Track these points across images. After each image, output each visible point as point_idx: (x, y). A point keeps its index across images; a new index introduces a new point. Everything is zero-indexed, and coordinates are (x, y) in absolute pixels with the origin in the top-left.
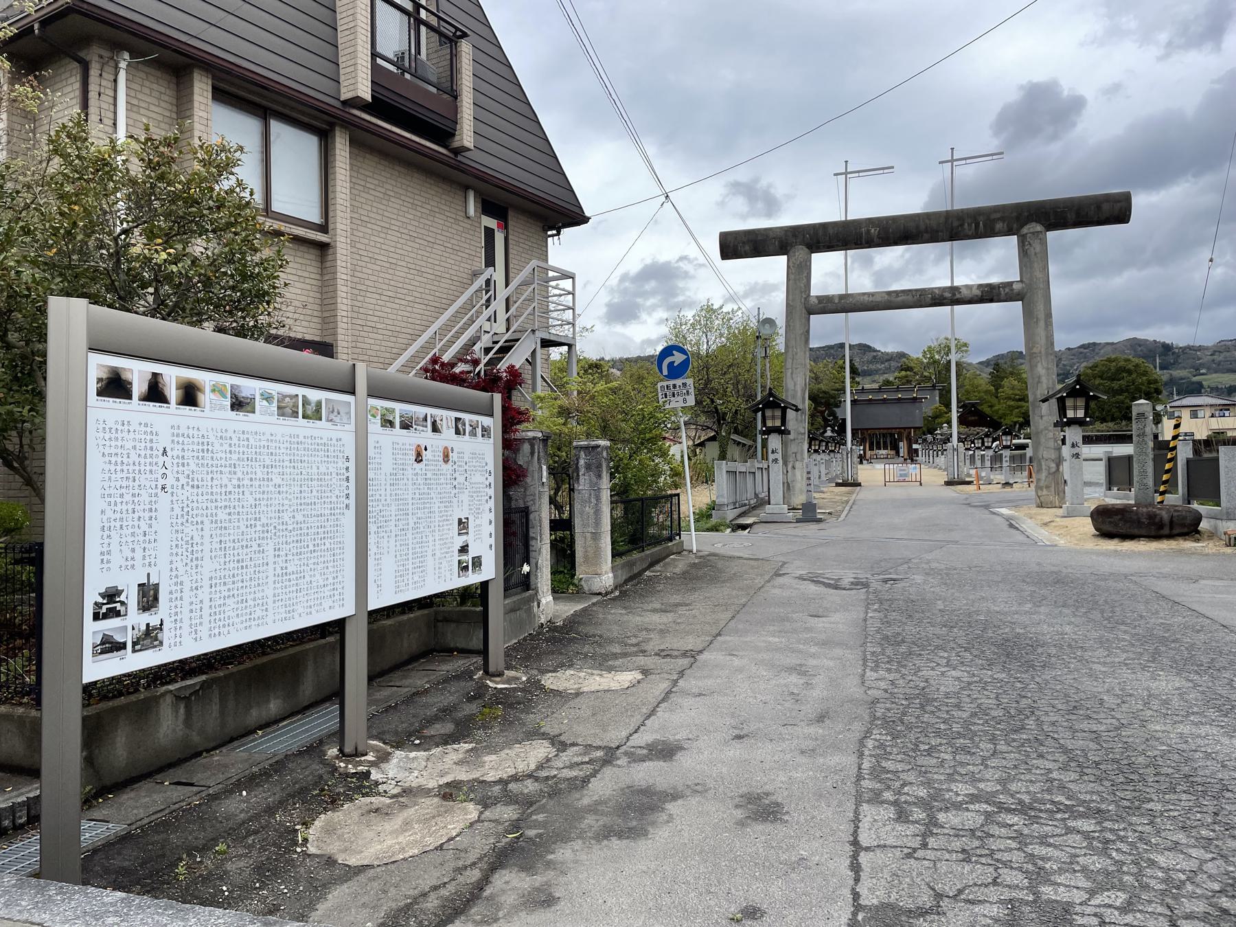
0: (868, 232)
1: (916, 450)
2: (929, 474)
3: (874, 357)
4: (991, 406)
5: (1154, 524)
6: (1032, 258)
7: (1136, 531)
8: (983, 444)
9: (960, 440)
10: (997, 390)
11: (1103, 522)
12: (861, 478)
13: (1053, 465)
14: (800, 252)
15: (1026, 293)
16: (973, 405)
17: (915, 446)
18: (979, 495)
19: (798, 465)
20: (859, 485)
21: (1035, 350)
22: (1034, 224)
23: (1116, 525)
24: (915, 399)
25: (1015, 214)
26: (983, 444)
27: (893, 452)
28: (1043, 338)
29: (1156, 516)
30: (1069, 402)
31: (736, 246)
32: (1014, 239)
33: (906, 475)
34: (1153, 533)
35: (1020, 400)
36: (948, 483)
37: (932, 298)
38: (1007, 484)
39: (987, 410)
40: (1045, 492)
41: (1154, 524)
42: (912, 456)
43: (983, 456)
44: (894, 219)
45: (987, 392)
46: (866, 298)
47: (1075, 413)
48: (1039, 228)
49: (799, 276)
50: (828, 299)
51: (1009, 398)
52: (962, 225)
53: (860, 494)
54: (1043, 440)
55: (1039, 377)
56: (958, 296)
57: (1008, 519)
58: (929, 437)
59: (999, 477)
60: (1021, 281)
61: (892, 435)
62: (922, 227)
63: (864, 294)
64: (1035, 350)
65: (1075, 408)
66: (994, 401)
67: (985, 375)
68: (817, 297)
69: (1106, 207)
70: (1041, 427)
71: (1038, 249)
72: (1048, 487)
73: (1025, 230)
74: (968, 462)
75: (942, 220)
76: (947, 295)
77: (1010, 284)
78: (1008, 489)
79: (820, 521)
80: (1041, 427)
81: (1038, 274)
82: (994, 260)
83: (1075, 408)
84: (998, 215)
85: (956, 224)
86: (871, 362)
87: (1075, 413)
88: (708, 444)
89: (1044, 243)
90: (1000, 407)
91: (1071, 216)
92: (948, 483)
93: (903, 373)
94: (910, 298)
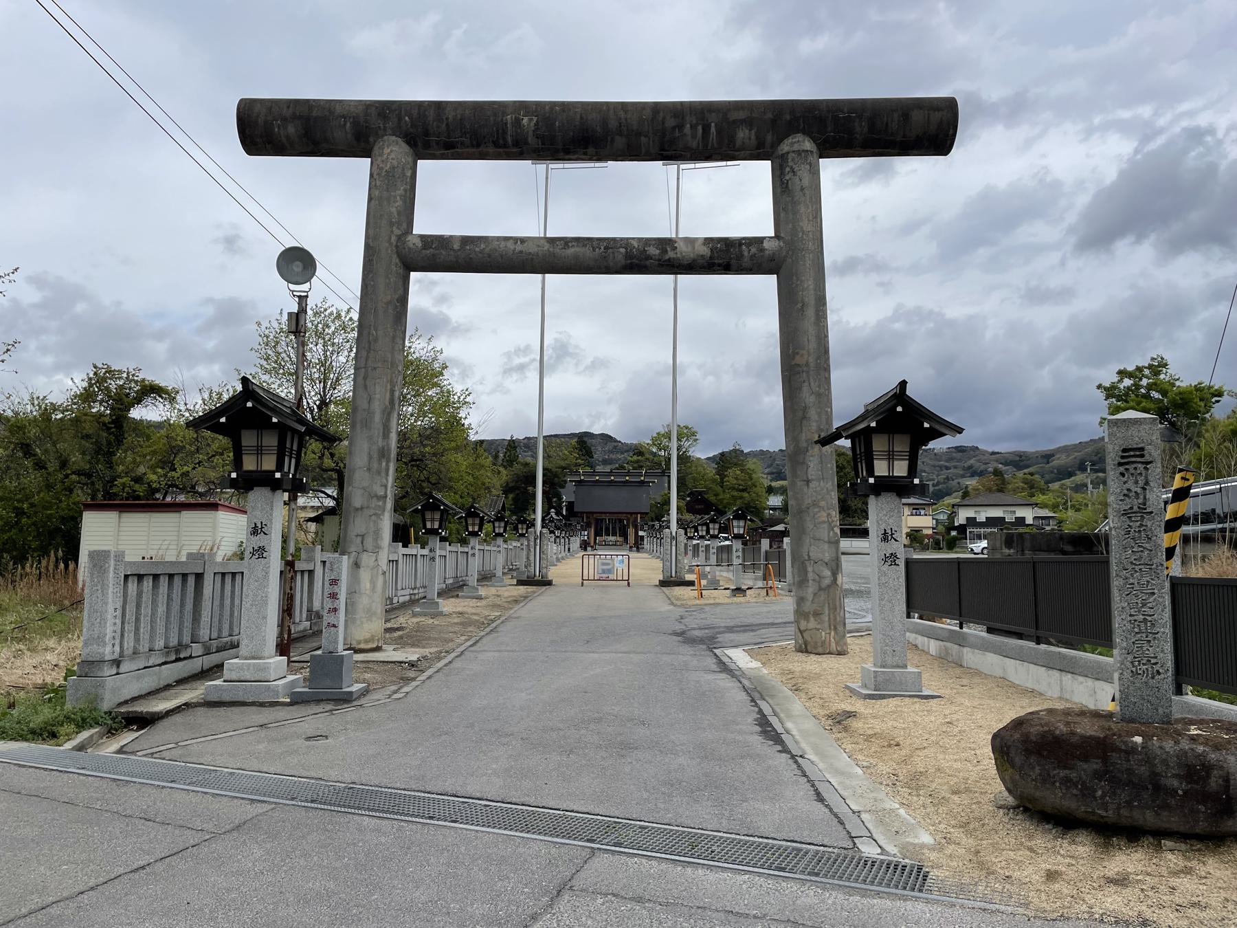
0: (518, 122)
1: (642, 537)
2: (644, 566)
3: (615, 447)
4: (716, 495)
5: (1205, 797)
6: (796, 200)
7: (1149, 818)
8: (708, 532)
9: (681, 524)
10: (722, 479)
11: (1046, 779)
12: (553, 573)
13: (827, 573)
14: (394, 150)
15: (787, 257)
16: (700, 493)
17: (641, 533)
18: (701, 609)
19: (366, 559)
20: (549, 583)
21: (798, 360)
22: (799, 137)
23: (1086, 793)
24: (642, 482)
25: (769, 115)
26: (708, 532)
27: (620, 539)
28: (813, 340)
29: (1208, 768)
30: (879, 444)
31: (273, 129)
32: (763, 169)
33: (609, 571)
34: (1201, 826)
35: (743, 490)
36: (664, 583)
37: (628, 256)
38: (738, 591)
39: (712, 498)
40: (812, 624)
41: (1205, 797)
42: (638, 545)
43: (707, 547)
44: (565, 106)
45: (714, 481)
46: (510, 245)
47: (891, 467)
48: (808, 145)
49: (390, 206)
50: (442, 242)
51: (734, 488)
52: (680, 127)
53: (542, 601)
54: (809, 525)
55: (805, 409)
56: (671, 254)
57: (755, 692)
58: (657, 525)
59: (725, 575)
60: (777, 236)
61: (621, 521)
62: (613, 124)
63: (507, 239)
64: (798, 360)
65: (891, 457)
66: (719, 489)
67: (711, 471)
68: (422, 237)
69: (917, 116)
70: (808, 501)
71: (806, 182)
72: (817, 614)
73: (785, 147)
74: (690, 553)
75: (647, 114)
76: (653, 251)
77: (760, 240)
78: (739, 599)
79: (346, 699)
80: (808, 501)
81: (806, 225)
82: (733, 198)
83: (891, 457)
84: (741, 115)
85: (671, 122)
86: (611, 452)
87: (891, 467)
88: (328, 519)
89: (815, 173)
90: (726, 496)
91: (860, 129)
92: (664, 583)
93: (635, 458)
94: (587, 252)
